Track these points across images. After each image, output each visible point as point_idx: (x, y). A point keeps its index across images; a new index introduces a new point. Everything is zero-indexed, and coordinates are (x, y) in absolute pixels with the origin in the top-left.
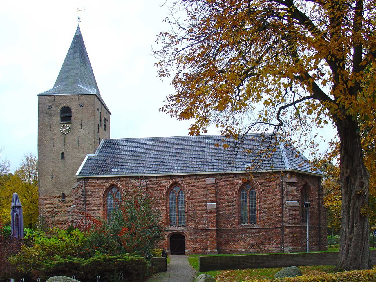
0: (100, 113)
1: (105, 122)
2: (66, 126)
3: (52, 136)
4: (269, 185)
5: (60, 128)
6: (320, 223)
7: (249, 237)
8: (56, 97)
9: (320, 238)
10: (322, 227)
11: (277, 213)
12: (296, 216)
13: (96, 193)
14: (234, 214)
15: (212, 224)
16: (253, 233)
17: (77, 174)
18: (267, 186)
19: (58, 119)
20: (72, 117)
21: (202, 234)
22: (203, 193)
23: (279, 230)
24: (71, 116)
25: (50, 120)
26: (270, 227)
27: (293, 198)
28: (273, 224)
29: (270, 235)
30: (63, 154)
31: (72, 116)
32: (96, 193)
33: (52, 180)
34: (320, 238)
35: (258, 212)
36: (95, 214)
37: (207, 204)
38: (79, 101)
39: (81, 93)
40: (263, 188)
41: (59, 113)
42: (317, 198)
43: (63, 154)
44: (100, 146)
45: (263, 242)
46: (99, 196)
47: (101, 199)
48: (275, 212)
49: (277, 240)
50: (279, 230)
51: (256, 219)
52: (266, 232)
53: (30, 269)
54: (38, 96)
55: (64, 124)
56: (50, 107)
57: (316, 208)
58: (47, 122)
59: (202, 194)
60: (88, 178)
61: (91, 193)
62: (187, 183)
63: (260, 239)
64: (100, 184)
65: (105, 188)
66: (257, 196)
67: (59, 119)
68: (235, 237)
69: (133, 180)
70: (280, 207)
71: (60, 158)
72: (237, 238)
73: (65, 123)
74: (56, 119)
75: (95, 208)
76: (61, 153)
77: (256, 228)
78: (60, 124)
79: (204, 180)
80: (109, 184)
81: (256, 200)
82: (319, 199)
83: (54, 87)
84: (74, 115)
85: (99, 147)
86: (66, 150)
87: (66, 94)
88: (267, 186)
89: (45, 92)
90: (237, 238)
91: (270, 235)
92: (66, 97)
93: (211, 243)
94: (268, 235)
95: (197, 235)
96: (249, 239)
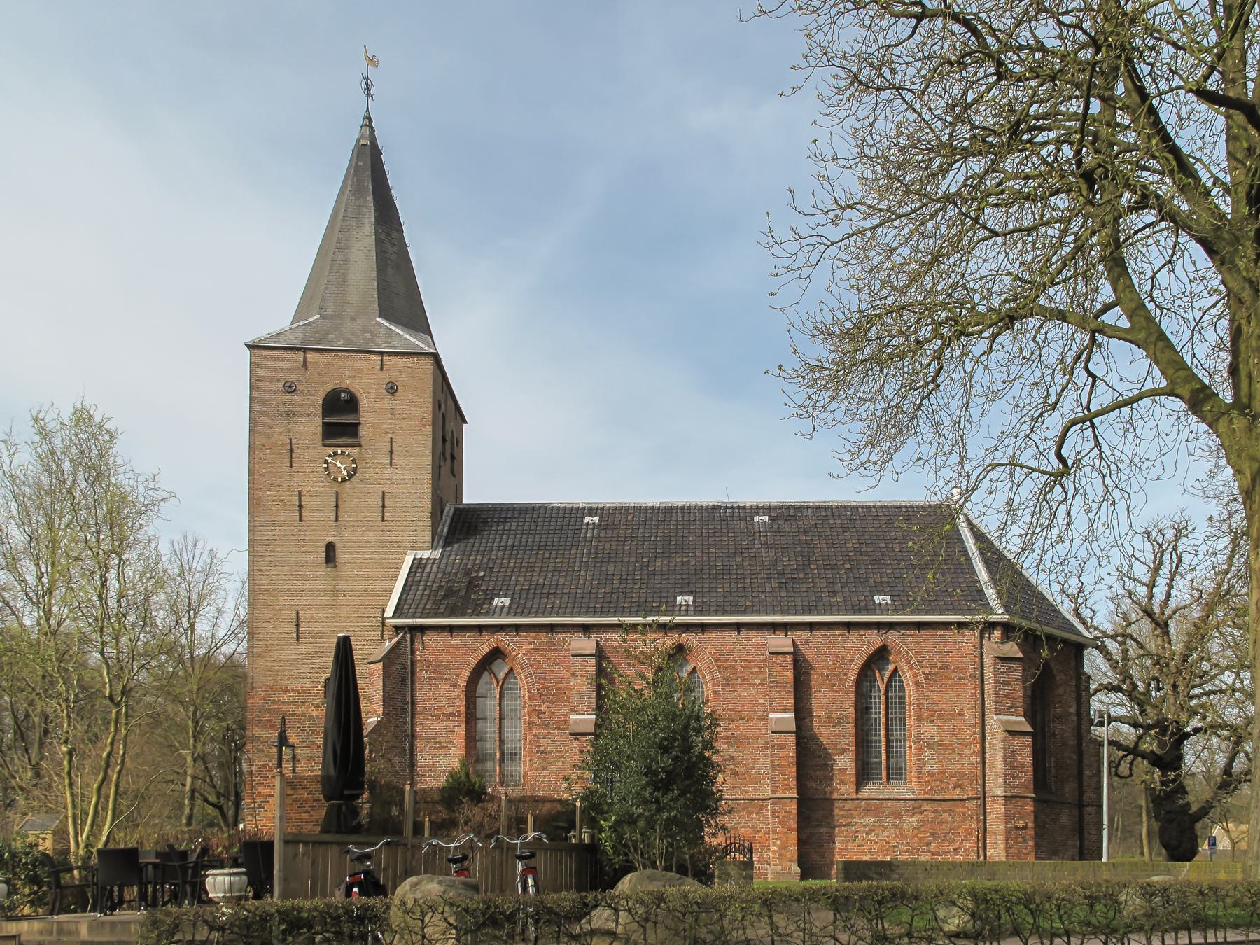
0: (443, 415)
1: (452, 448)
2: (343, 453)
3: (296, 485)
4: (945, 664)
5: (322, 461)
6: (1081, 793)
7: (885, 828)
8: (309, 355)
9: (1081, 839)
10: (1088, 806)
11: (967, 752)
12: (1022, 765)
13: (446, 677)
14: (845, 751)
15: (785, 780)
16: (899, 815)
17: (389, 612)
18: (939, 664)
19: (364, 405)
20: (361, 427)
21: (752, 813)
22: (757, 681)
23: (972, 805)
24: (359, 424)
25: (289, 431)
26: (947, 796)
27: (1012, 707)
28: (955, 788)
29: (946, 822)
30: (330, 548)
31: (362, 421)
32: (446, 677)
33: (295, 635)
34: (1081, 839)
35: (910, 747)
36: (441, 748)
37: (771, 715)
38: (383, 375)
39: (391, 348)
40: (927, 670)
41: (320, 412)
42: (1073, 710)
43: (330, 548)
44: (444, 526)
45: (928, 844)
46: (454, 686)
47: (459, 695)
48: (962, 750)
49: (966, 839)
50: (972, 805)
51: (905, 769)
52: (936, 812)
53: (1101, 179)
54: (249, 347)
55: (334, 449)
56: (290, 388)
57: (1072, 742)
58: (280, 437)
59: (755, 686)
60: (422, 629)
61: (430, 678)
62: (713, 650)
63: (920, 832)
64: (456, 648)
65: (474, 660)
66: (910, 696)
67: (320, 429)
68: (848, 825)
69: (558, 636)
70: (975, 733)
71: (323, 562)
72: (854, 829)
73: (339, 446)
74: (310, 427)
75: (439, 725)
76: (324, 545)
77: (908, 797)
78: (325, 445)
79: (759, 640)
80: (486, 649)
81: (904, 708)
82: (1079, 714)
83: (293, 322)
84: (368, 418)
85: (440, 527)
86: (340, 535)
87: (339, 346)
88: (939, 664)
89: (271, 337)
90: (854, 829)
91: (946, 822)
92: (341, 355)
93: (782, 842)
94: (941, 823)
95: (740, 817)
96: (886, 833)
